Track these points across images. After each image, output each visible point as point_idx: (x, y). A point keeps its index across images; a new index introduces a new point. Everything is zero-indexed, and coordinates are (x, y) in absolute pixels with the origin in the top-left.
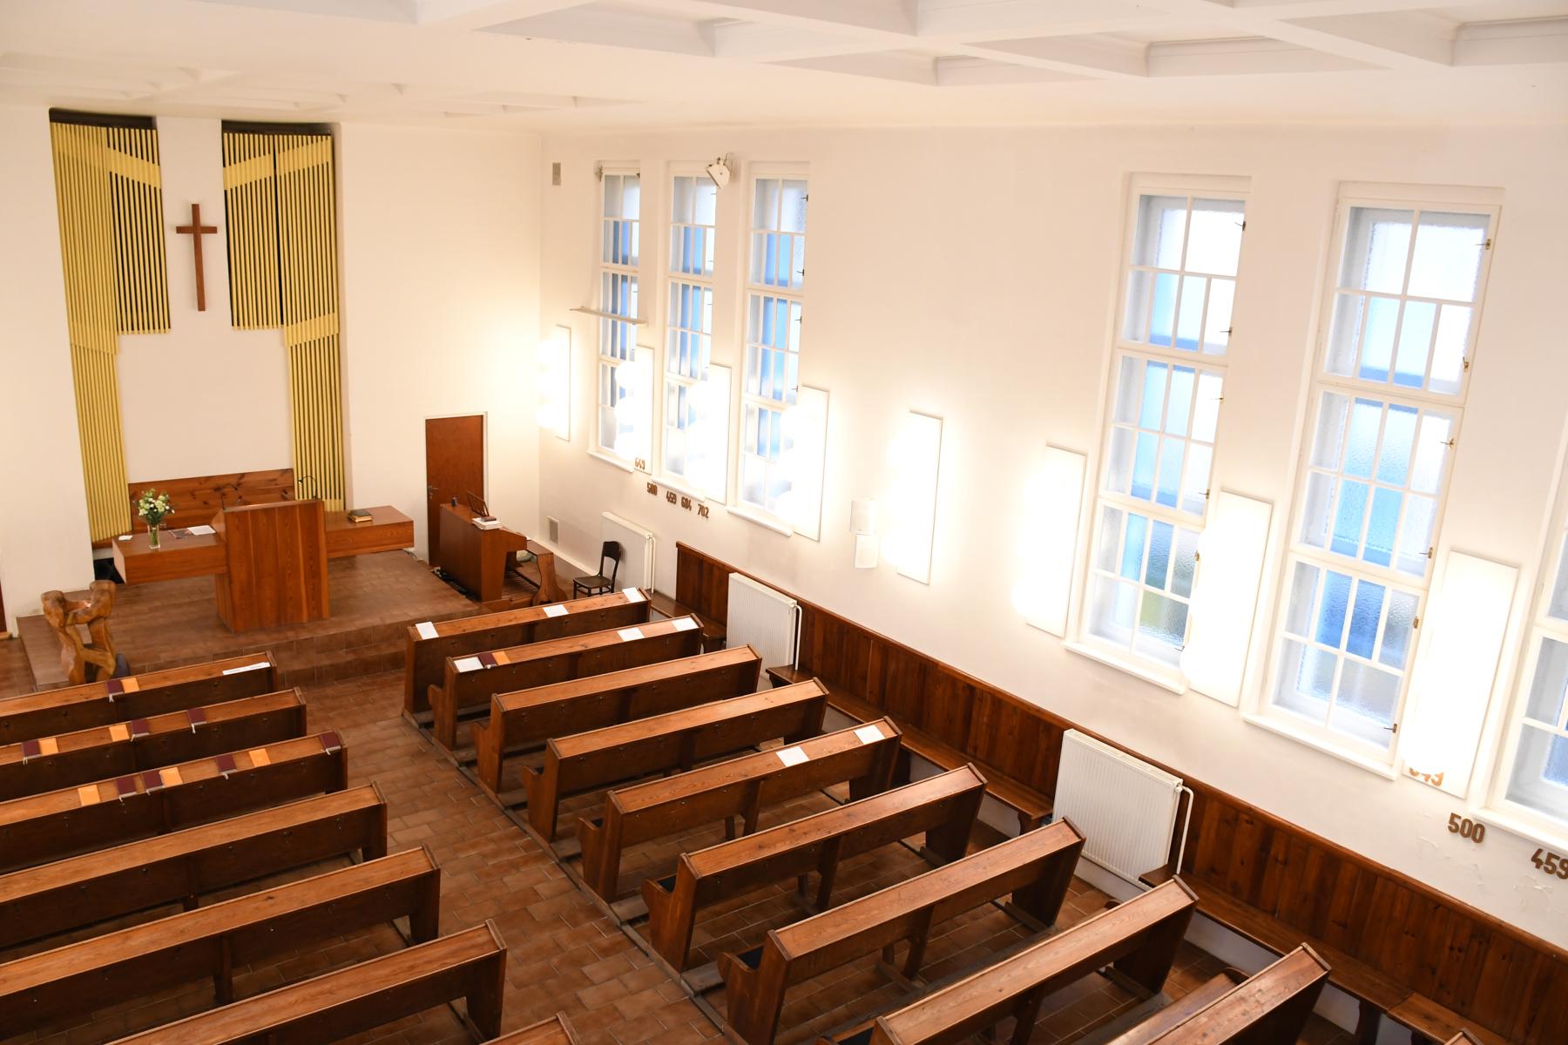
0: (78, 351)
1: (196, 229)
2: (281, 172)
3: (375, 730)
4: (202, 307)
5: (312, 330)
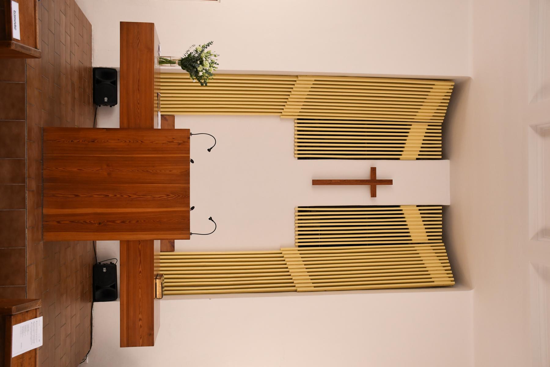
0: (285, 82)
1: (373, 182)
2: (418, 247)
4: (316, 182)
5: (297, 267)
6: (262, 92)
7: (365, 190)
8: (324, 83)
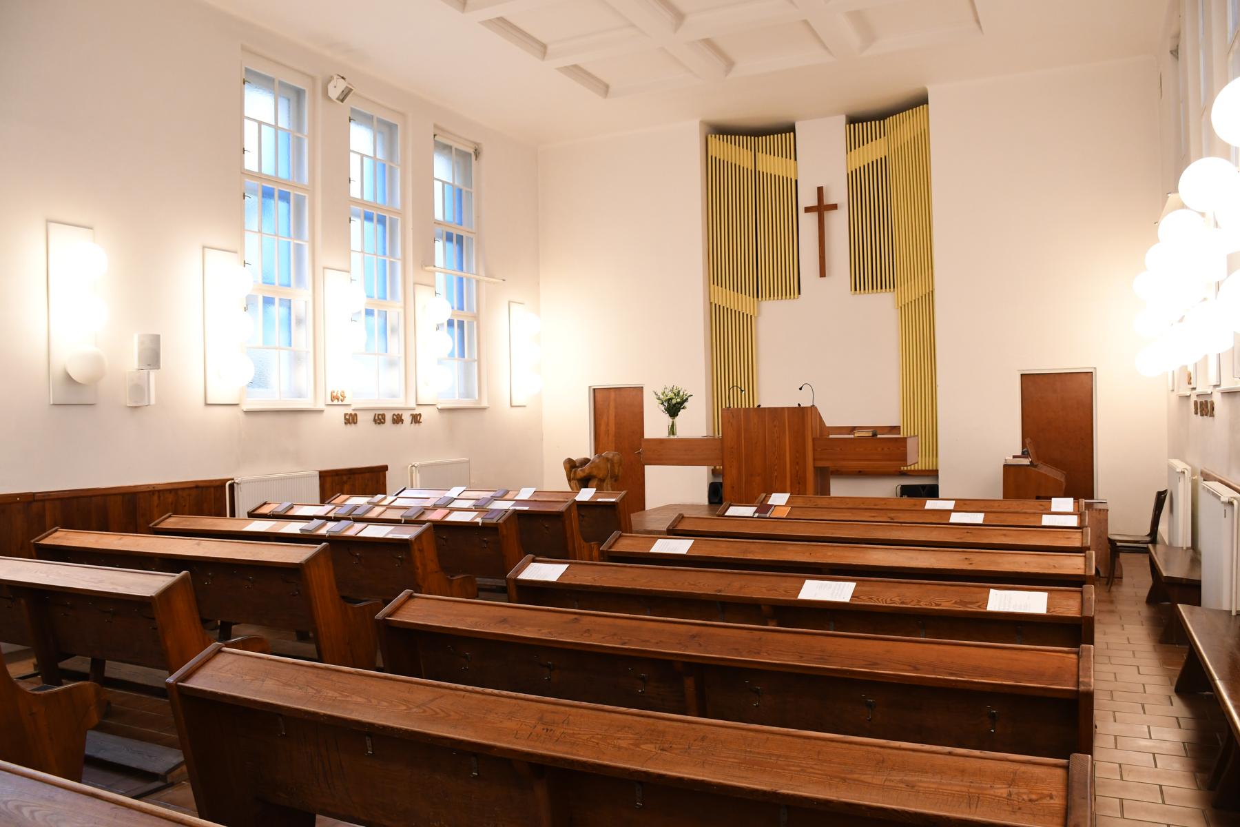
1: (822, 208)
3: (1071, 602)
4: (823, 273)
6: (730, 340)
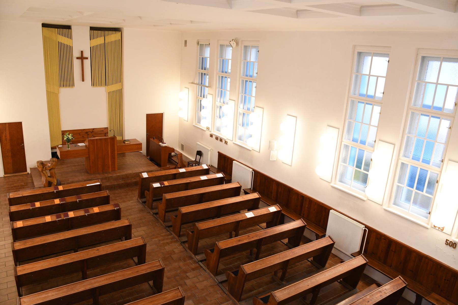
0: (48, 93)
1: (82, 58)
2: (106, 42)
4: (83, 80)
7: (85, 61)
8: (48, 82)
